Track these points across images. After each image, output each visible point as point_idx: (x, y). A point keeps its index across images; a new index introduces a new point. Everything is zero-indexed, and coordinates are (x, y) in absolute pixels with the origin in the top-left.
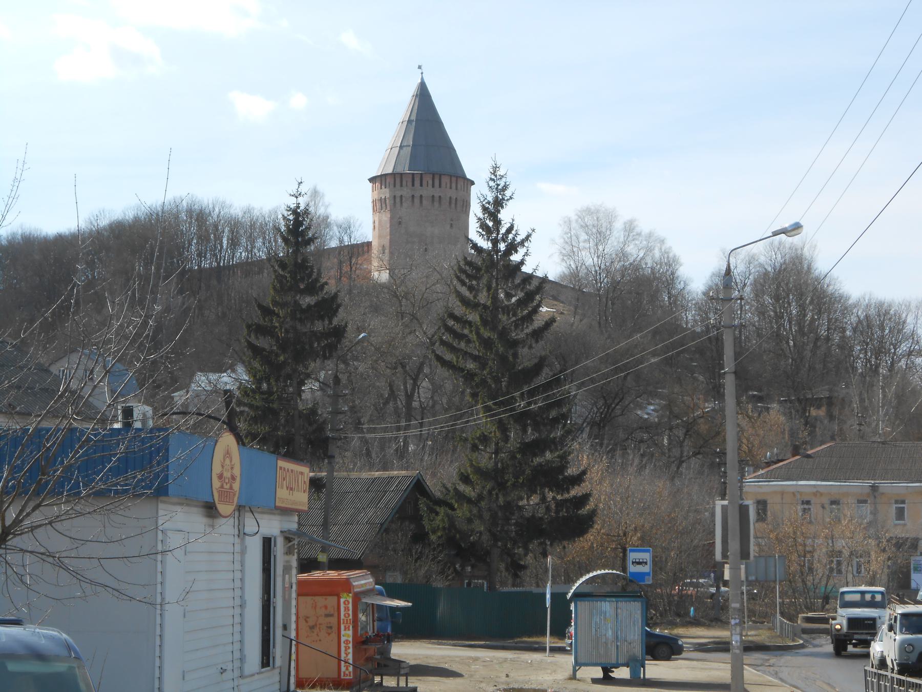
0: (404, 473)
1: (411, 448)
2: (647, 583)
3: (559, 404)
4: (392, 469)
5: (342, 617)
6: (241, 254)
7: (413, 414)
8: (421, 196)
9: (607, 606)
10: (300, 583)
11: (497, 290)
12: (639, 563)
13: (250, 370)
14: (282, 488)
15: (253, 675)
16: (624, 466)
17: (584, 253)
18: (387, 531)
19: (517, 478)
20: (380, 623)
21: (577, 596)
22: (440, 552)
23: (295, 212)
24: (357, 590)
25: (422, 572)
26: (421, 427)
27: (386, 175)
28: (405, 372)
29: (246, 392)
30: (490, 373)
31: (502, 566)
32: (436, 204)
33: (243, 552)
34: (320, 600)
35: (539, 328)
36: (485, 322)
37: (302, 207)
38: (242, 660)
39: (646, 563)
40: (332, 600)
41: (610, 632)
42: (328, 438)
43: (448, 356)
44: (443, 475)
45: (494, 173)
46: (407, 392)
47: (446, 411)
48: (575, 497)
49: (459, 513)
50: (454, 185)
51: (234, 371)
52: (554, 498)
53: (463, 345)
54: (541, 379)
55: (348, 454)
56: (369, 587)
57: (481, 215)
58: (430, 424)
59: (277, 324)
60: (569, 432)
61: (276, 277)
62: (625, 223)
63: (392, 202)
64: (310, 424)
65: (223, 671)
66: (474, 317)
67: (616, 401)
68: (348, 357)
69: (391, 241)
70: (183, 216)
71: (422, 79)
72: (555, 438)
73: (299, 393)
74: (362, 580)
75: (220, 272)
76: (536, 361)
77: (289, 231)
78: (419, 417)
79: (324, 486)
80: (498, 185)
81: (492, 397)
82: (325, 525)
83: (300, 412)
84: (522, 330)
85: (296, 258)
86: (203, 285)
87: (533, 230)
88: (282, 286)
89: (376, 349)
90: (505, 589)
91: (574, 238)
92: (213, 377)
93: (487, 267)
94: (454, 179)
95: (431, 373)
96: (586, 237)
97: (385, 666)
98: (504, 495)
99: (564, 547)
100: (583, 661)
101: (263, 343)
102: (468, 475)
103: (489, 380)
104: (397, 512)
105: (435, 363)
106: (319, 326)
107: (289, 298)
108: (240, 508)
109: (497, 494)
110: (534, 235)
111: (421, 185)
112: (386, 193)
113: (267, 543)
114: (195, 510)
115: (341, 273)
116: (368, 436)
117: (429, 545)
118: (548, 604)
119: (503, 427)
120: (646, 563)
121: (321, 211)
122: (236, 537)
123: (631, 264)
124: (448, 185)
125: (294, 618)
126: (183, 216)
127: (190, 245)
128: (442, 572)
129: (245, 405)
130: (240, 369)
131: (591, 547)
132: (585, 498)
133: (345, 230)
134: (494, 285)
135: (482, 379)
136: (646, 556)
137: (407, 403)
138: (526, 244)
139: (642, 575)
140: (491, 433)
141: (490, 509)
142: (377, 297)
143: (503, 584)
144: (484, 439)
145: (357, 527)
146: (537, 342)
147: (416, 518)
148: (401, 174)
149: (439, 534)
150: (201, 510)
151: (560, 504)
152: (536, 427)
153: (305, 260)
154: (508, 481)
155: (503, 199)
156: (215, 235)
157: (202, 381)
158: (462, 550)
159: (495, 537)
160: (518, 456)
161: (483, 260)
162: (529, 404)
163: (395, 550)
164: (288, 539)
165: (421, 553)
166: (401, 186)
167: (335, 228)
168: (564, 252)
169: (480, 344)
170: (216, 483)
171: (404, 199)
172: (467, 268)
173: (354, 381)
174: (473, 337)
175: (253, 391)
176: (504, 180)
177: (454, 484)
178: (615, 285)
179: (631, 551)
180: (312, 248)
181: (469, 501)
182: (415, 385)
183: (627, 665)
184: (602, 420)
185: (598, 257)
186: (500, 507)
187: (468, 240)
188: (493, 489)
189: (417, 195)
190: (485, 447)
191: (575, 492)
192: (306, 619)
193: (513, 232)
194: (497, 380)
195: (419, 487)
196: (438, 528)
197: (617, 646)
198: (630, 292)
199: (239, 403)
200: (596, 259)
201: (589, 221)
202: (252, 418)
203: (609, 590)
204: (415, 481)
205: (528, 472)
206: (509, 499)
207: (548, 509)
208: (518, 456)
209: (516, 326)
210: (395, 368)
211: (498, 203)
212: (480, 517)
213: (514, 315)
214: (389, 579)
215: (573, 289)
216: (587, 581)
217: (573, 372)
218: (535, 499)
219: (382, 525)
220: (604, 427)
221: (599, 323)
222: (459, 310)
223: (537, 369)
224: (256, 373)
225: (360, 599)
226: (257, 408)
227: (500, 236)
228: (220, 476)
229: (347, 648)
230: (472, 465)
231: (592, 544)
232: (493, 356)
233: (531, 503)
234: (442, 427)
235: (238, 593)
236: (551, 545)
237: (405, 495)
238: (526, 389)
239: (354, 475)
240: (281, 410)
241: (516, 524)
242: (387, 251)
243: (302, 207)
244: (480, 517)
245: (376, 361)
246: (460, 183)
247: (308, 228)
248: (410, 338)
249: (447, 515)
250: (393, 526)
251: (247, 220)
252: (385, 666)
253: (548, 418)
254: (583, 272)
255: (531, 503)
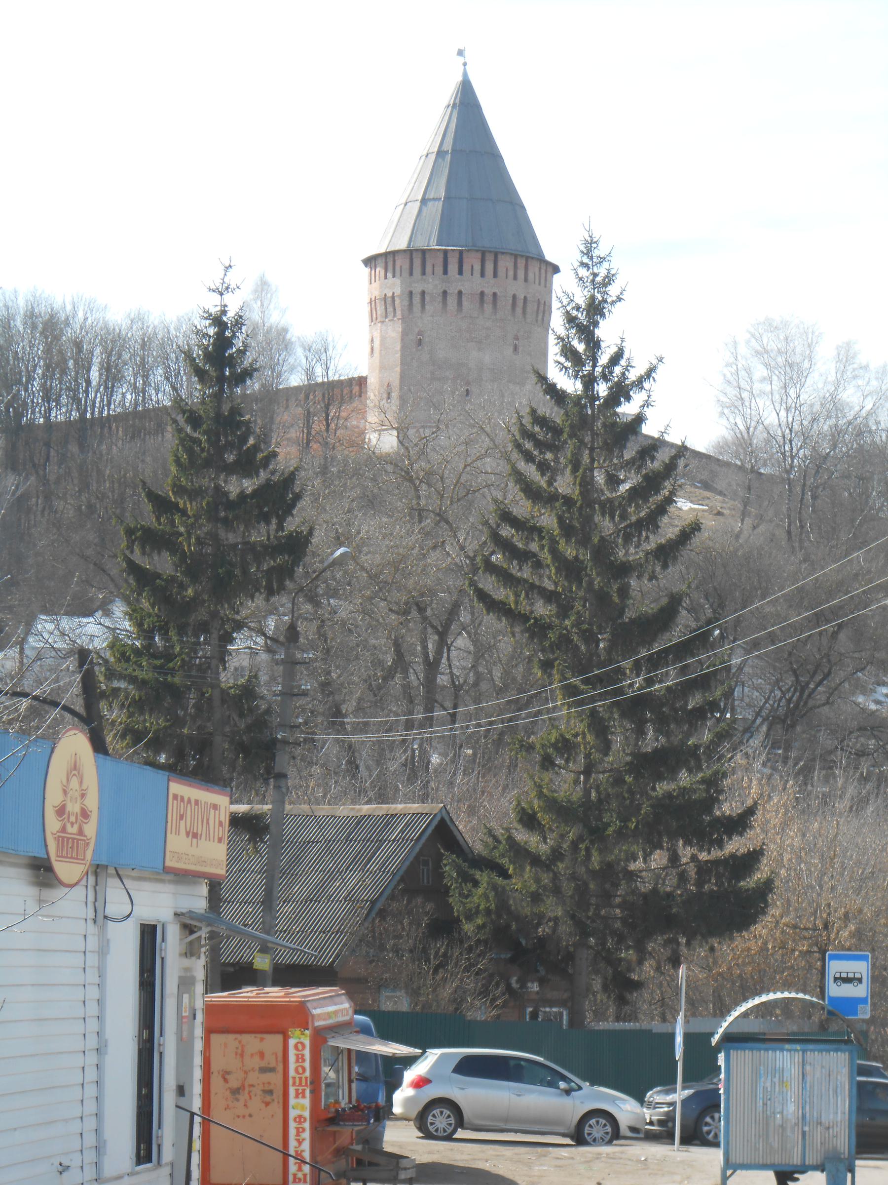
0: (415, 807)
1: (435, 759)
2: (860, 1016)
3: (704, 682)
4: (394, 801)
5: (292, 1073)
6: (125, 397)
7: (438, 697)
8: (495, 294)
9: (786, 1060)
10: (211, 1010)
11: (592, 470)
12: (847, 980)
13: (135, 615)
14: (178, 833)
15: (119, 1177)
16: (825, 800)
17: (761, 402)
18: (382, 914)
19: (625, 820)
20: (364, 1085)
21: (730, 1039)
22: (482, 954)
23: (218, 321)
24: (319, 1023)
25: (447, 992)
26: (454, 722)
27: (394, 253)
28: (425, 619)
29: (123, 654)
30: (577, 624)
31: (597, 984)
32: (488, 308)
33: (103, 950)
34: (251, 1042)
35: (670, 541)
36: (567, 530)
37: (231, 314)
38: (99, 1149)
39: (860, 980)
40: (273, 1042)
41: (791, 1108)
42: (275, 741)
43: (501, 593)
44: (487, 813)
45: (588, 253)
46: (426, 656)
47: (500, 692)
48: (733, 856)
49: (516, 883)
50: (521, 274)
51: (108, 613)
52: (694, 858)
53: (526, 573)
54: (676, 635)
55: (316, 770)
56: (341, 1019)
57: (562, 332)
58: (469, 717)
59: (182, 529)
60: (721, 736)
61: (182, 441)
62: (838, 348)
63: (406, 303)
64: (241, 715)
65: (63, 1169)
66: (548, 520)
67: (818, 678)
68: (320, 591)
69: (403, 377)
70: (19, 323)
71: (465, 74)
72: (697, 747)
73: (222, 656)
74: (330, 1005)
75: (84, 430)
76: (664, 601)
77: (208, 356)
78: (448, 704)
79: (266, 829)
80: (595, 275)
81: (581, 668)
82: (268, 902)
83: (224, 692)
84: (638, 546)
85: (219, 406)
86: (52, 453)
87: (660, 360)
88: (193, 460)
89: (370, 577)
90: (602, 1026)
91: (742, 373)
92: (66, 623)
93: (572, 426)
94: (521, 263)
95: (473, 621)
96: (765, 373)
97: (371, 1164)
98: (601, 851)
99: (712, 949)
100: (739, 1160)
101: (163, 564)
102: (535, 814)
103: (575, 638)
104: (402, 880)
105: (479, 606)
106: (259, 535)
107: (205, 482)
108: (98, 870)
109: (587, 850)
110: (661, 368)
111: (460, 272)
112: (395, 286)
113: (149, 935)
114: (12, 871)
115: (309, 433)
116: (354, 738)
117: (462, 942)
118: (679, 1054)
119: (599, 727)
120: (860, 980)
121: (274, 319)
122: (90, 923)
123: (850, 423)
124: (511, 273)
125: (198, 1074)
126: (18, 323)
127: (30, 379)
128: (484, 992)
129: (121, 677)
130: (119, 609)
131: (764, 948)
132: (753, 858)
133: (318, 353)
134: (586, 459)
135: (561, 635)
136: (861, 968)
137: (427, 677)
138: (646, 385)
139: (853, 1003)
140: (576, 735)
141: (573, 877)
142: (374, 480)
143: (600, 1015)
144: (565, 746)
145: (326, 906)
146: (665, 566)
147: (438, 892)
148: (424, 252)
149: (480, 921)
150: (26, 873)
151: (704, 870)
152: (662, 724)
153: (235, 411)
154: (608, 825)
155: (605, 301)
156: (76, 363)
157: (49, 632)
158: (521, 952)
159: (583, 930)
160: (629, 779)
161: (567, 414)
162: (650, 682)
163: (396, 950)
164: (188, 929)
165: (445, 955)
166: (424, 273)
167: (299, 352)
168: (725, 399)
169: (558, 569)
170: (53, 824)
171: (427, 298)
172: (537, 429)
173: (330, 635)
174: (546, 556)
175: (137, 652)
176: (605, 265)
177: (507, 830)
178: (819, 462)
179: (833, 957)
180: (257, 386)
181: (535, 860)
182: (443, 643)
183: (821, 1168)
184: (790, 713)
185: (788, 410)
186: (593, 873)
187: (542, 378)
188: (581, 839)
189: (453, 290)
190: (567, 761)
191: (735, 846)
192: (225, 1075)
193: (623, 362)
194: (590, 638)
195: (443, 833)
196: (477, 912)
197: (804, 1134)
198: (846, 476)
199: (111, 675)
200: (783, 414)
201: (772, 342)
202: (134, 701)
203: (795, 1028)
204: (435, 823)
205: (645, 809)
206: (611, 858)
207: (682, 877)
208: (629, 779)
209: (627, 539)
210: (406, 612)
211: (596, 309)
212: (557, 890)
213: (623, 517)
214: (387, 1005)
215: (741, 468)
216: (745, 1015)
217: (738, 621)
218: (659, 859)
219: (373, 903)
220: (793, 726)
221: (789, 533)
222: (522, 508)
223: (666, 616)
224: (142, 619)
225: (325, 1041)
226: (144, 682)
227: (599, 369)
228: (61, 811)
229: (299, 1131)
230: (540, 795)
231: (765, 943)
232: (581, 593)
233: (651, 865)
234: (491, 723)
235: (93, 1025)
236: (688, 944)
237: (417, 849)
238: (644, 653)
239: (323, 810)
240: (189, 688)
241: (622, 906)
242: (395, 395)
243: (231, 314)
244: (557, 890)
245: (371, 598)
246: (534, 268)
247: (242, 352)
248: (433, 557)
249: (495, 887)
250: (395, 905)
251: (137, 333)
252: (371, 1164)
253: (684, 708)
254: (759, 437)
255: (651, 865)
